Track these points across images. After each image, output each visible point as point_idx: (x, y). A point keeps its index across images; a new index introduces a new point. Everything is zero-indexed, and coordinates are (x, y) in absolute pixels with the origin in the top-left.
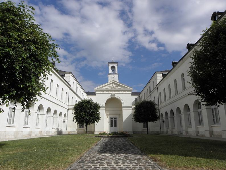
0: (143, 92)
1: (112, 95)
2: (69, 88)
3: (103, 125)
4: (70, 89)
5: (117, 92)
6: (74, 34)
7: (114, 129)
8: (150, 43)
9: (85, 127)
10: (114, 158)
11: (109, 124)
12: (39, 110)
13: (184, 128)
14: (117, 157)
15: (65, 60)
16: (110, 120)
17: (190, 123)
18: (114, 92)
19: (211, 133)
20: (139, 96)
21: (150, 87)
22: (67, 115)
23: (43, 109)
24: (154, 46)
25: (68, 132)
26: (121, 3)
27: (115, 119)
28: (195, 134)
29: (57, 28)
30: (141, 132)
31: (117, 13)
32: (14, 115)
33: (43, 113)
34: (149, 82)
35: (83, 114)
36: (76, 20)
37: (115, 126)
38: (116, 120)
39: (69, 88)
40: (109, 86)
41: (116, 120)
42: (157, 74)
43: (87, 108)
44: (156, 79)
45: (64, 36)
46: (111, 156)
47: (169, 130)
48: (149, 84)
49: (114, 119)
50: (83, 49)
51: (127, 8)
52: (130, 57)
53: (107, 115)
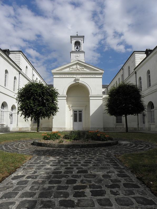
1: (75, 80)
2: (19, 72)
3: (63, 120)
5: (83, 76)
6: (46, 36)
7: (81, 127)
8: (118, 45)
11: (72, 118)
12: (3, 107)
15: (38, 61)
16: (73, 113)
18: (78, 76)
20: (107, 89)
21: (123, 75)
23: (8, 107)
24: (122, 48)
25: (20, 128)
26: (94, 3)
27: (79, 111)
29: (31, 29)
30: (113, 128)
31: (90, 14)
32: (12, 118)
33: (8, 110)
34: (122, 68)
35: (30, 103)
36: (50, 21)
37: (80, 120)
38: (81, 113)
40: (72, 67)
41: (81, 113)
42: (135, 54)
43: (36, 94)
44: (134, 62)
45: (36, 38)
48: (122, 71)
49: (78, 112)
50: (55, 51)
51: (99, 9)
52: (99, 58)
53: (69, 107)
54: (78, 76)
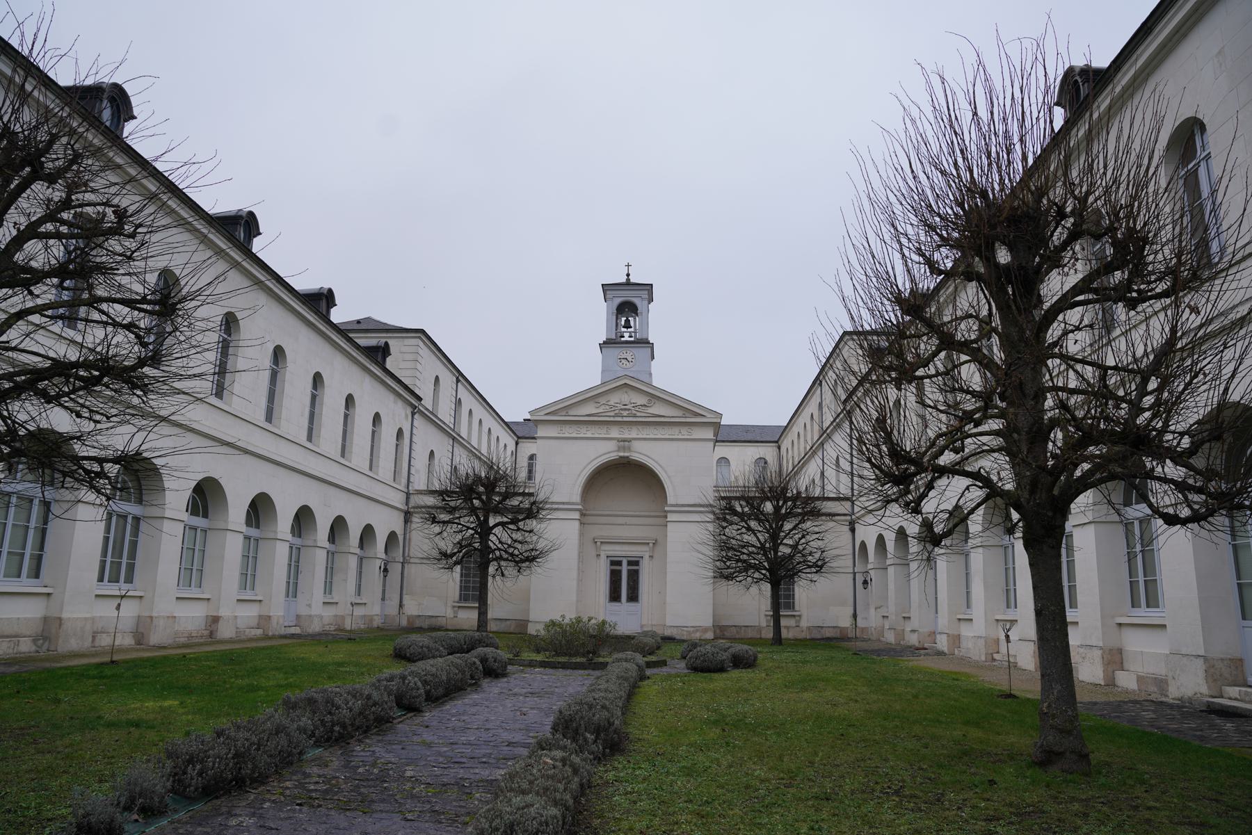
0: (797, 428)
2: (454, 439)
4: (415, 410)
13: (943, 621)
20: (779, 448)
21: (820, 405)
22: (401, 538)
25: (409, 617)
28: (983, 651)
37: (633, 597)
40: (602, 400)
54: (633, 433)
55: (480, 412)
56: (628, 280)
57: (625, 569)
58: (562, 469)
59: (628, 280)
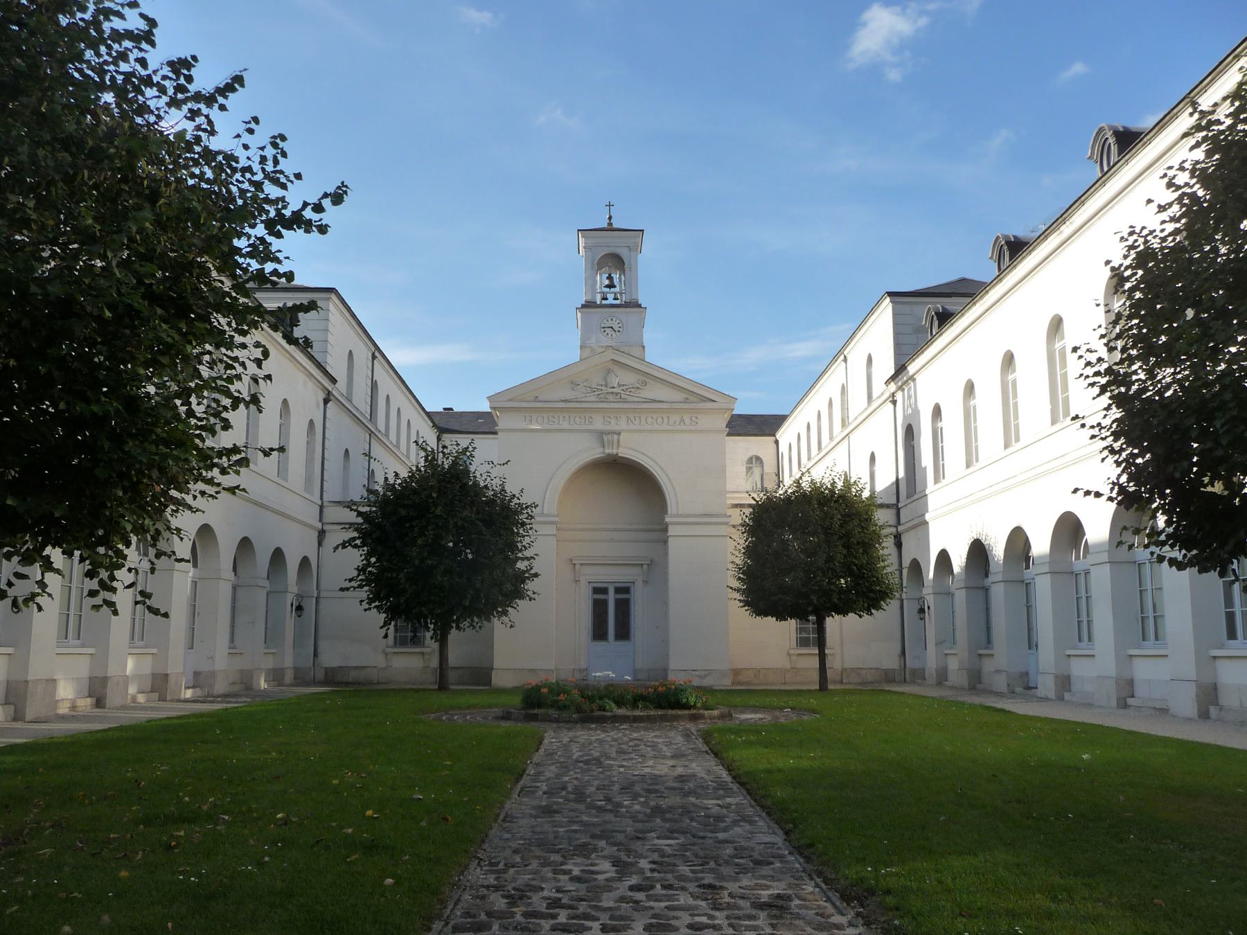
2: (371, 433)
9: (432, 645)
10: (640, 896)
13: (1046, 656)
14: (658, 886)
17: (1085, 625)
19: (1209, 697)
20: (777, 442)
21: (844, 390)
27: (618, 590)
37: (624, 632)
39: (329, 393)
46: (620, 879)
47: (953, 664)
55: (399, 399)
56: (610, 224)
57: (611, 597)
58: (528, 469)
59: (610, 224)
